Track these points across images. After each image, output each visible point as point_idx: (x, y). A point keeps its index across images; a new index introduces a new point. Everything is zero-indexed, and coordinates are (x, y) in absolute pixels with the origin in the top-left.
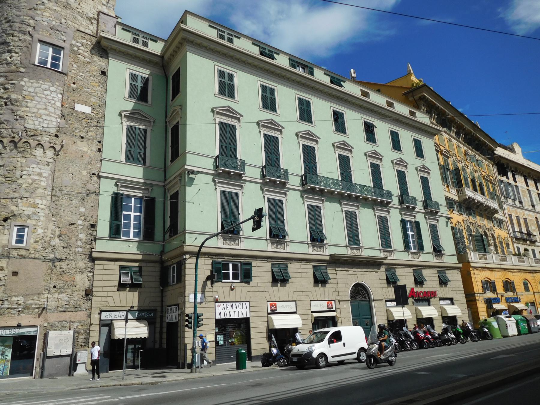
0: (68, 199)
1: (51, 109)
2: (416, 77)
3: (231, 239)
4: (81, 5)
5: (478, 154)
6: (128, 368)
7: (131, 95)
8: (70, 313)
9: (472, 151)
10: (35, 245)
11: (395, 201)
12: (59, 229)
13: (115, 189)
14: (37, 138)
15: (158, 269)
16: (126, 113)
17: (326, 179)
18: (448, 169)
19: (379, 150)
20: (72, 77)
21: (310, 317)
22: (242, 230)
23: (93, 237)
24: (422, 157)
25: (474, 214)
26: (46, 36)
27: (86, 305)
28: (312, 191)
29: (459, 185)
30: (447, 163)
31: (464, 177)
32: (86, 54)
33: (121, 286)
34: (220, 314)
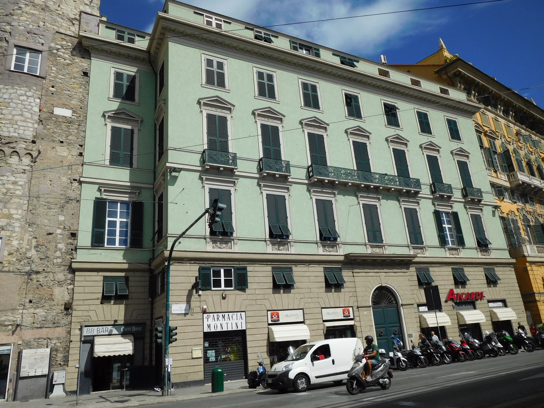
0: (46, 207)
1: (28, 115)
2: (450, 52)
3: (222, 242)
4: (61, 6)
5: (533, 134)
6: (114, 388)
7: (117, 94)
8: (47, 329)
9: (525, 130)
10: (10, 258)
11: (425, 191)
12: (36, 240)
13: (98, 195)
14: (12, 145)
15: (147, 279)
16: (110, 114)
17: (337, 170)
18: (495, 153)
19: (464, 147)
20: (50, 80)
21: (321, 327)
22: (290, 234)
23: (73, 247)
24: (430, 132)
25: (533, 201)
26: (23, 41)
27: (65, 321)
28: (321, 184)
29: (509, 168)
30: (493, 145)
31: (517, 160)
32: (66, 56)
33: (105, 299)
34: (209, 326)
